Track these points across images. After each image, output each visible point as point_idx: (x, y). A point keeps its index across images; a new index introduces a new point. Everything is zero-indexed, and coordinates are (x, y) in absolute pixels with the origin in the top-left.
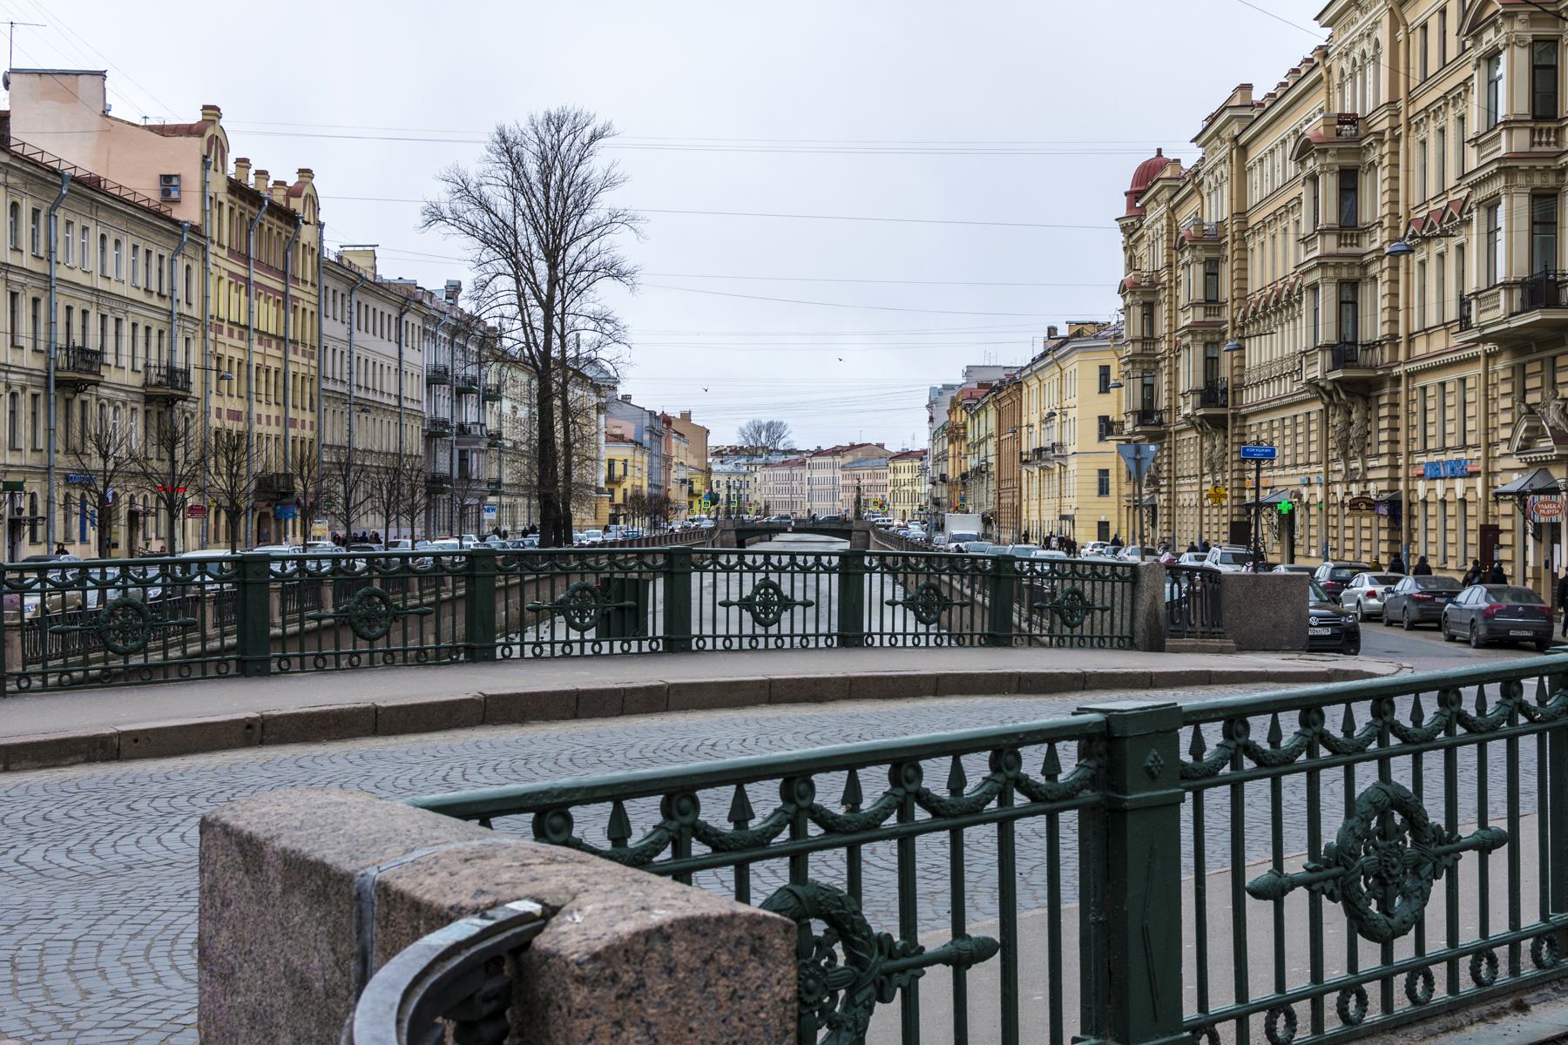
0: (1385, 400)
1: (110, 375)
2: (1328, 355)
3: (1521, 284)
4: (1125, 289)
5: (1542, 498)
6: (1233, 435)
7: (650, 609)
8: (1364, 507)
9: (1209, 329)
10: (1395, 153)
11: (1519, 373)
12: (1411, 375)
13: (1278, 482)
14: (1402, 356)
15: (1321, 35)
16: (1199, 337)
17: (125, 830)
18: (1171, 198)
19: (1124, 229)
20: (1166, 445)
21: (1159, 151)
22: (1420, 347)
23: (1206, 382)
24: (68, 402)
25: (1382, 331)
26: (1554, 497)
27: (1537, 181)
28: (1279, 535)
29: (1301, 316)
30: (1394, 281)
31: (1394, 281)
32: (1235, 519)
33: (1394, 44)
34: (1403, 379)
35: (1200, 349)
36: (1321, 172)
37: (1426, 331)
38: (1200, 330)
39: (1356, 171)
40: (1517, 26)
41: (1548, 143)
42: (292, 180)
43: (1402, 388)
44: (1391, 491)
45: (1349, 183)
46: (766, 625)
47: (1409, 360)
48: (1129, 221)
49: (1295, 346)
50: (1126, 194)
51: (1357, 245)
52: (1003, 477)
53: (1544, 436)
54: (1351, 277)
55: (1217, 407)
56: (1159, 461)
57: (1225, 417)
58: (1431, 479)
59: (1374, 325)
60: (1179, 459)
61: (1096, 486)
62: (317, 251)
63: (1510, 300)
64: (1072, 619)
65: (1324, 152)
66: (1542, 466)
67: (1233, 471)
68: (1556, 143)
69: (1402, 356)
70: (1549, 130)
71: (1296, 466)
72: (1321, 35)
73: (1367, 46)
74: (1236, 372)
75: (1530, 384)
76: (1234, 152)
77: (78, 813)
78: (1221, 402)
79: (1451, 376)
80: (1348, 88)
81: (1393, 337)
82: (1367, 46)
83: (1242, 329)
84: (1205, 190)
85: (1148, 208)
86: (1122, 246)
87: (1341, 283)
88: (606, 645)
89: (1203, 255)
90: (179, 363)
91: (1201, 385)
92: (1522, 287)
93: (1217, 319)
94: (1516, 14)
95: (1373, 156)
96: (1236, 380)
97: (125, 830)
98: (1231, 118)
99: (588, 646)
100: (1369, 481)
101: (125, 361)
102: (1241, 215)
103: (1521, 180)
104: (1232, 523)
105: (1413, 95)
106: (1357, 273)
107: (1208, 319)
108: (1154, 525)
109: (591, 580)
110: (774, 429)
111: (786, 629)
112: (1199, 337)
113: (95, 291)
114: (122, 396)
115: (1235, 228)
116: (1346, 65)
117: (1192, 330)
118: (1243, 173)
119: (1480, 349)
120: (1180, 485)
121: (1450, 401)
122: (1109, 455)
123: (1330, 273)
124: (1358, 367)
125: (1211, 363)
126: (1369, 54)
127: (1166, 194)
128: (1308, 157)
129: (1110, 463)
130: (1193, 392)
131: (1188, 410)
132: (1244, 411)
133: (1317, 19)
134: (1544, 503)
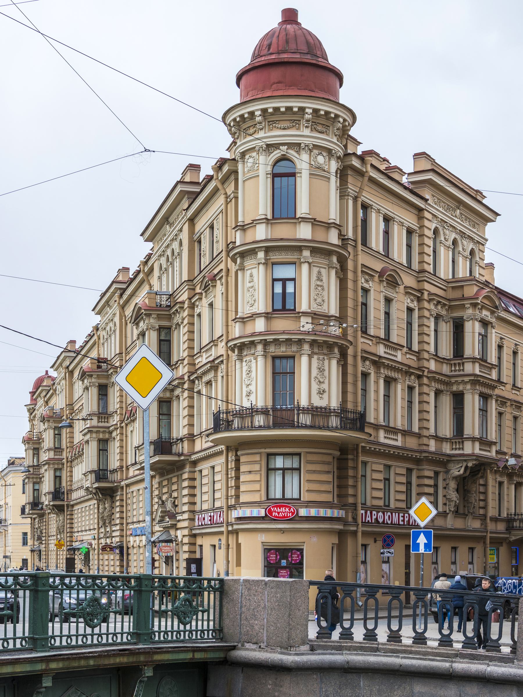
2: (93, 475)
4: (25, 441)
5: (163, 544)
6: (67, 515)
7: (131, 624)
8: (109, 550)
9: (57, 462)
12: (128, 486)
13: (85, 538)
15: (97, 319)
16: (51, 466)
18: (45, 396)
19: (29, 410)
20: (44, 520)
23: (55, 489)
25: (117, 464)
26: (169, 544)
28: (85, 564)
32: (68, 556)
35: (52, 472)
36: (90, 386)
38: (52, 462)
39: (107, 386)
40: (152, 321)
44: (121, 542)
47: (127, 479)
48: (31, 407)
51: (107, 422)
54: (104, 438)
56: (42, 528)
59: (114, 463)
60: (50, 527)
61: (21, 541)
64: (185, 618)
65: (91, 376)
67: (67, 533)
72: (97, 319)
74: (68, 483)
76: (67, 374)
83: (71, 462)
85: (38, 400)
86: (28, 419)
87: (100, 441)
89: (53, 425)
91: (52, 490)
92: (154, 445)
93: (60, 457)
96: (69, 488)
98: (65, 357)
100: (113, 537)
104: (67, 559)
105: (128, 350)
106: (107, 436)
107: (56, 457)
108: (40, 560)
111: (104, 630)
112: (51, 466)
115: (68, 412)
117: (48, 462)
120: (51, 540)
122: (26, 524)
123: (94, 435)
124: (109, 482)
125: (58, 478)
126: (113, 329)
127: (44, 393)
128: (85, 378)
129: (28, 530)
130: (49, 493)
132: (72, 503)
133: (93, 310)
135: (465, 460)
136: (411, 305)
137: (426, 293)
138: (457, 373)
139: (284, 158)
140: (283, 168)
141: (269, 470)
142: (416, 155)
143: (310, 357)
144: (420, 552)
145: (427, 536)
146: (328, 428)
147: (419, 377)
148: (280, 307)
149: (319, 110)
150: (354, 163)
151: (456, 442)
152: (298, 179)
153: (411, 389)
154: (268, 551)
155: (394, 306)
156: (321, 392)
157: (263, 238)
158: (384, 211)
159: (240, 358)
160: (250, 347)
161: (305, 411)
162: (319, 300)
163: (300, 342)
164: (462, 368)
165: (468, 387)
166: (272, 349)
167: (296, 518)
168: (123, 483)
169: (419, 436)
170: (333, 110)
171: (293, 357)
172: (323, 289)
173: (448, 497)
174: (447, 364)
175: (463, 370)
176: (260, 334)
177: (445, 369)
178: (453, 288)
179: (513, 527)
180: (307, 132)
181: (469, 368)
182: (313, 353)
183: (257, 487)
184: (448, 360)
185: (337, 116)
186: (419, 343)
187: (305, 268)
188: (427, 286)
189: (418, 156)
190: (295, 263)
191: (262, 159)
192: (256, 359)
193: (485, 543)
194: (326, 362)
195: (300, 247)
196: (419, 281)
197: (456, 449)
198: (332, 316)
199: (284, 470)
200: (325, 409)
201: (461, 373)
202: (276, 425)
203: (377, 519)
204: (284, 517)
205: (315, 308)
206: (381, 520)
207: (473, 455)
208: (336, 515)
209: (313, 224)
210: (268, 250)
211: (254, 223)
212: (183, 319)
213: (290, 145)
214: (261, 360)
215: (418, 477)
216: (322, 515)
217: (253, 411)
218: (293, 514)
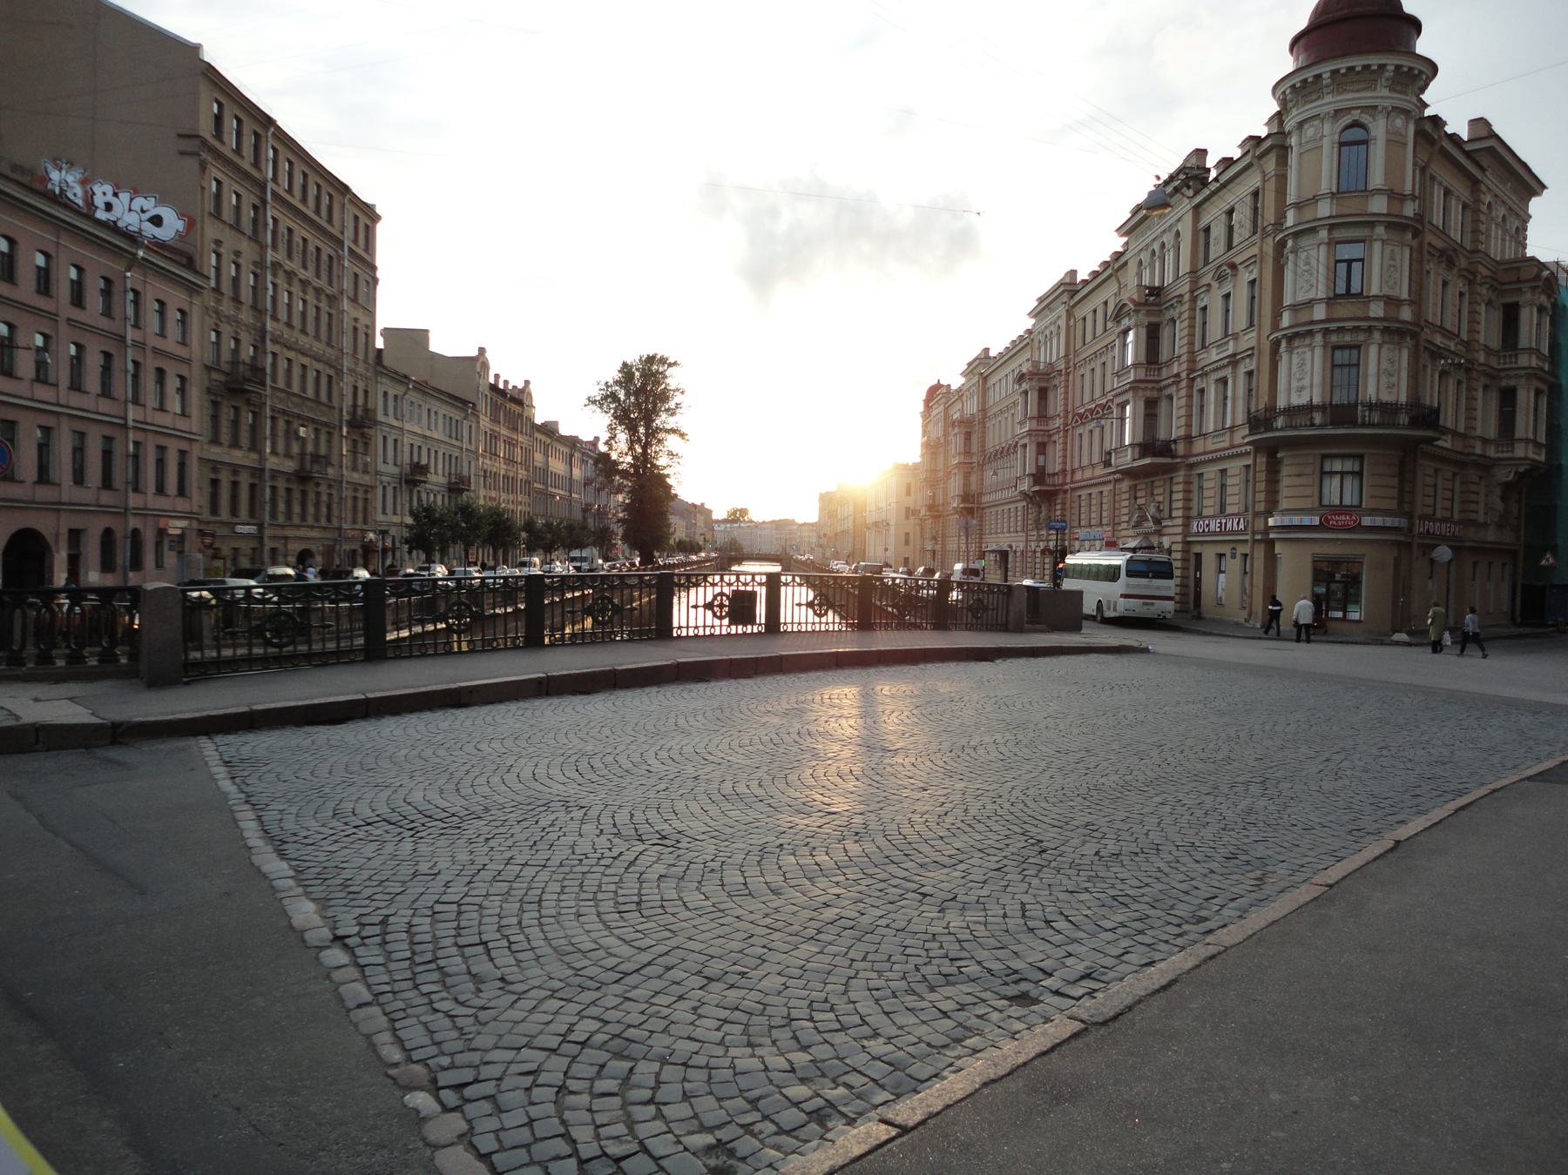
1: (432, 478)
3: (1140, 445)
10: (1067, 381)
11: (1134, 489)
12: (1074, 489)
14: (1068, 480)
17: (476, 771)
22: (1078, 476)
24: (411, 492)
25: (1058, 468)
27: (1148, 394)
30: (1065, 443)
31: (1065, 443)
33: (1068, 328)
37: (1082, 468)
42: (521, 385)
45: (1043, 394)
46: (820, 616)
47: (1072, 482)
53: (1147, 520)
62: (530, 420)
63: (1133, 453)
66: (1146, 535)
69: (1068, 480)
73: (1053, 328)
75: (1176, 488)
77: (442, 753)
79: (1094, 491)
80: (1043, 349)
81: (1064, 471)
82: (1053, 328)
84: (964, 398)
88: (733, 627)
90: (465, 472)
95: (1056, 382)
97: (476, 771)
99: (724, 629)
101: (440, 472)
103: (1140, 392)
106: (1046, 439)
109: (726, 590)
110: (744, 512)
113: (425, 437)
114: (437, 488)
116: (1041, 338)
118: (985, 391)
119: (1111, 477)
121: (1094, 502)
139: (1356, 124)
140: (1357, 134)
141: (1323, 473)
143: (1380, 346)
152: (1372, 147)
153: (1459, 382)
154: (1316, 562)
155: (1450, 289)
157: (1328, 214)
158: (1446, 184)
159: (1290, 350)
161: (1371, 406)
163: (1370, 330)
165: (1523, 381)
166: (1334, 338)
167: (1359, 528)
168: (1066, 487)
169: (1464, 436)
171: (1358, 347)
176: (1321, 322)
180: (1385, 92)
181: (1523, 360)
182: (1384, 342)
183: (1308, 491)
185: (1421, 72)
187: (1377, 246)
190: (1363, 241)
191: (1327, 127)
192: (1313, 350)
195: (1373, 222)
199: (1342, 474)
202: (1335, 423)
205: (1386, 291)
207: (1526, 458)
208: (1396, 525)
209: (1389, 197)
210: (1332, 227)
211: (1315, 199)
212: (1181, 314)
213: (1364, 109)
214: (1318, 352)
215: (1462, 483)
217: (1309, 408)
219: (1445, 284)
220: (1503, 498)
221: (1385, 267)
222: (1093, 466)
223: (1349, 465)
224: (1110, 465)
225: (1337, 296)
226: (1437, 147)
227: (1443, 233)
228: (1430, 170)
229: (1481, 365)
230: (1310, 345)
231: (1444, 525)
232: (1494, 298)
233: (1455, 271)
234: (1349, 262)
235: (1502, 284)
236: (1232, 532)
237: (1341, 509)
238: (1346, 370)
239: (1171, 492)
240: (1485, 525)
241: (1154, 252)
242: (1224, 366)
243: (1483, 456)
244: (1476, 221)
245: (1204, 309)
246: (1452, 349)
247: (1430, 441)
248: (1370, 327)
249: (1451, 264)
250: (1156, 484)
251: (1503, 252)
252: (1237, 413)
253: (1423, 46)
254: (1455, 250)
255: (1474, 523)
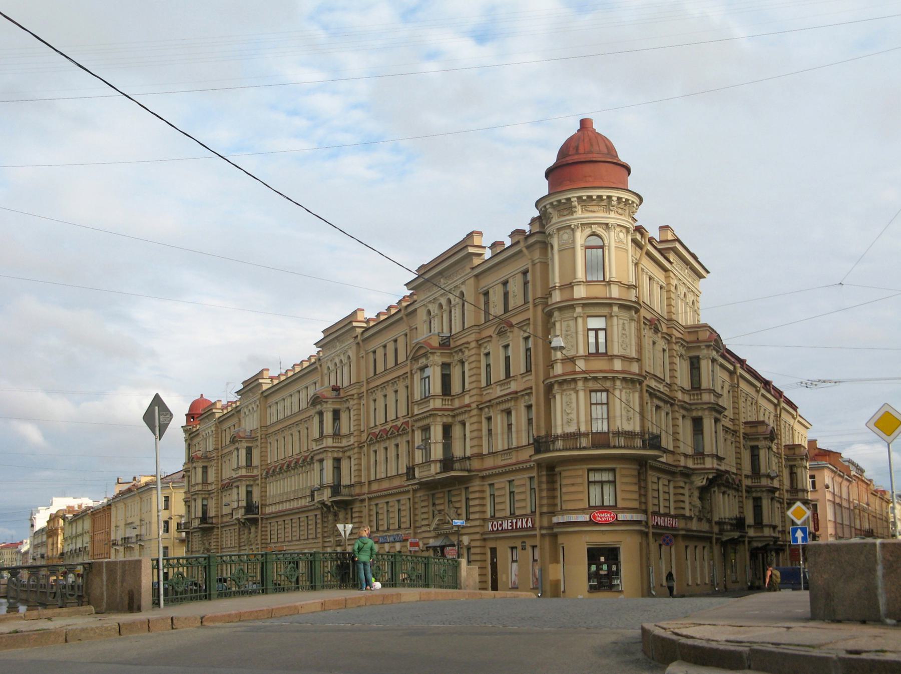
0: (215, 533)
5: (450, 548)
21: (202, 395)
27: (445, 420)
29: (314, 470)
34: (260, 521)
41: (448, 405)
43: (220, 530)
49: (299, 486)
50: (186, 415)
51: (341, 442)
52: (96, 553)
55: (253, 514)
57: (258, 519)
58: (382, 543)
68: (451, 405)
70: (448, 399)
71: (300, 540)
78: (256, 512)
79: (303, 516)
94: (435, 353)
102: (264, 427)
103: (244, 482)
124: (342, 496)
131: (239, 516)
134: (452, 550)
135: (706, 473)
136: (665, 347)
137: (674, 337)
138: (696, 401)
140: (595, 241)
142: (660, 227)
144: (799, 543)
145: (804, 530)
146: (634, 448)
147: (672, 405)
148: (594, 351)
149: (622, 198)
150: (637, 237)
151: (697, 458)
153: (667, 414)
156: (629, 419)
158: (650, 273)
160: (570, 383)
162: (624, 346)
163: (614, 379)
164: (699, 397)
170: (625, 195)
172: (626, 337)
173: (693, 504)
174: (687, 394)
175: (701, 399)
177: (686, 398)
178: (689, 332)
179: (724, 529)
184: (688, 391)
185: (633, 202)
186: (670, 377)
188: (675, 332)
189: (664, 228)
192: (577, 392)
193: (711, 543)
194: (631, 394)
196: (668, 328)
197: (698, 464)
198: (634, 358)
200: (632, 432)
201: (699, 401)
203: (657, 523)
204: (606, 521)
206: (659, 524)
207: (712, 469)
215: (675, 487)
216: (635, 519)
218: (613, 518)
219: (654, 343)
220: (701, 498)
221: (620, 334)
222: (238, 468)
223: (606, 476)
224: (414, 477)
225: (590, 354)
226: (644, 251)
227: (650, 309)
228: (640, 266)
229: (679, 401)
230: (573, 389)
231: (666, 519)
232: (684, 352)
233: (659, 335)
234: (597, 331)
235: (687, 342)
236: (522, 529)
237: (602, 508)
238: (599, 407)
239: (467, 499)
240: (691, 518)
241: (441, 306)
242: (508, 400)
243: (685, 467)
244: (669, 298)
245: (488, 354)
246: (662, 390)
247: (655, 458)
248: (614, 377)
249: (656, 331)
250: (437, 496)
251: (686, 320)
252: (521, 438)
253: (633, 183)
254: (658, 320)
255: (684, 517)
